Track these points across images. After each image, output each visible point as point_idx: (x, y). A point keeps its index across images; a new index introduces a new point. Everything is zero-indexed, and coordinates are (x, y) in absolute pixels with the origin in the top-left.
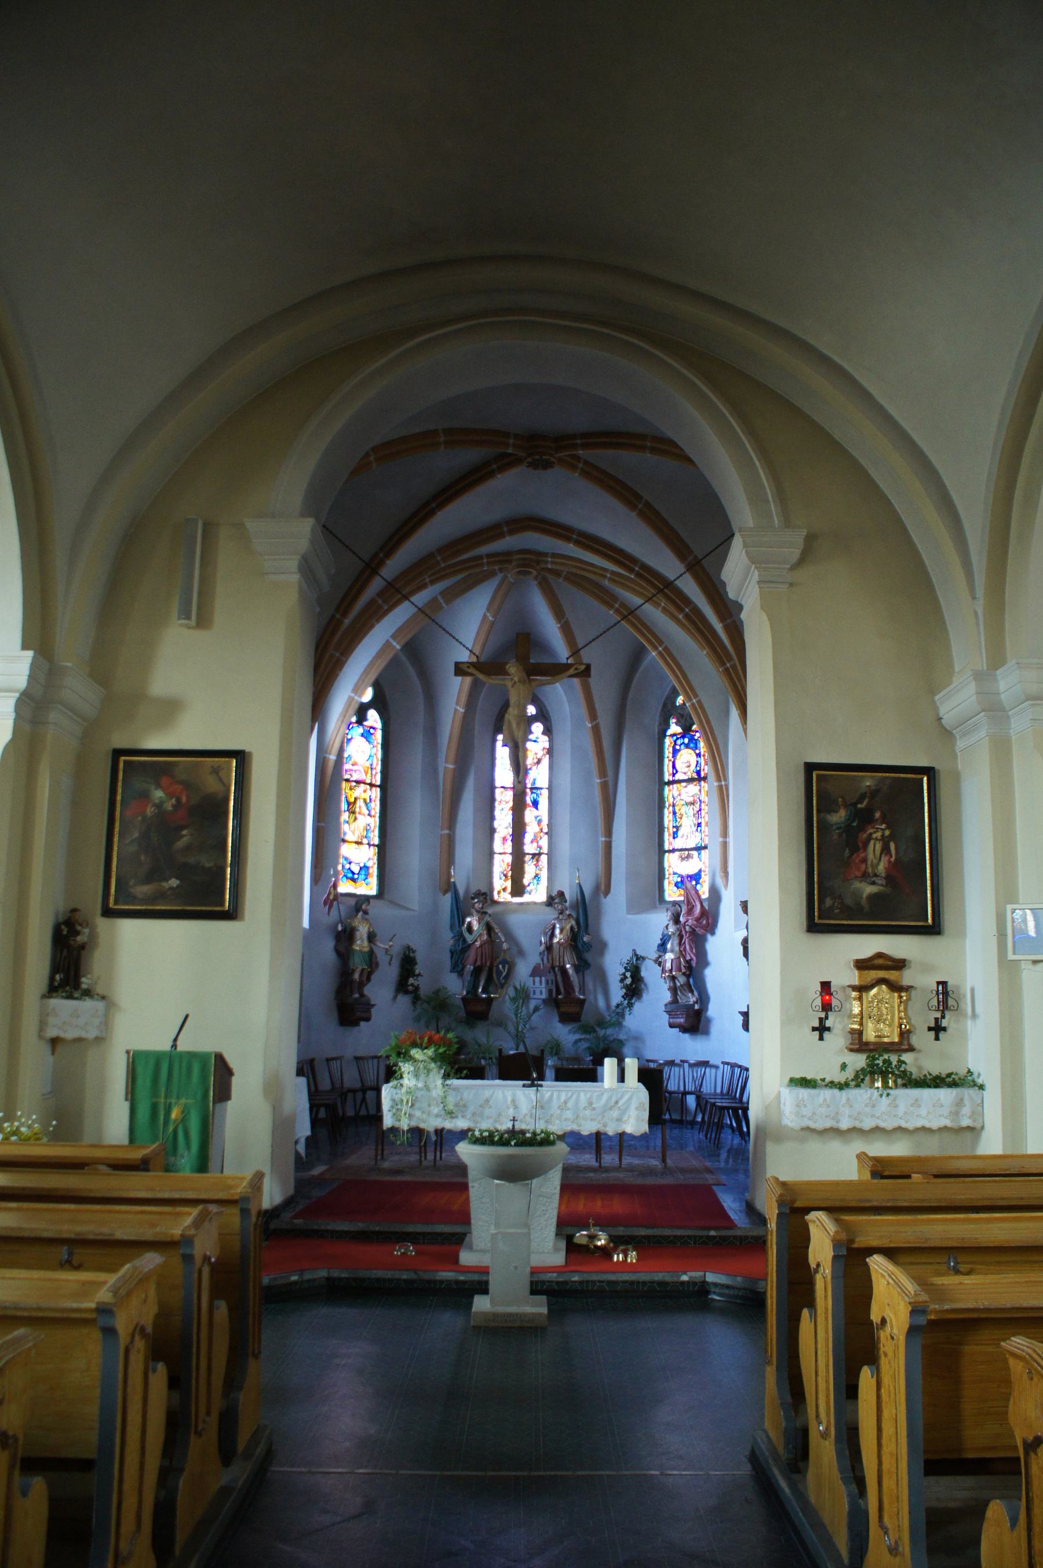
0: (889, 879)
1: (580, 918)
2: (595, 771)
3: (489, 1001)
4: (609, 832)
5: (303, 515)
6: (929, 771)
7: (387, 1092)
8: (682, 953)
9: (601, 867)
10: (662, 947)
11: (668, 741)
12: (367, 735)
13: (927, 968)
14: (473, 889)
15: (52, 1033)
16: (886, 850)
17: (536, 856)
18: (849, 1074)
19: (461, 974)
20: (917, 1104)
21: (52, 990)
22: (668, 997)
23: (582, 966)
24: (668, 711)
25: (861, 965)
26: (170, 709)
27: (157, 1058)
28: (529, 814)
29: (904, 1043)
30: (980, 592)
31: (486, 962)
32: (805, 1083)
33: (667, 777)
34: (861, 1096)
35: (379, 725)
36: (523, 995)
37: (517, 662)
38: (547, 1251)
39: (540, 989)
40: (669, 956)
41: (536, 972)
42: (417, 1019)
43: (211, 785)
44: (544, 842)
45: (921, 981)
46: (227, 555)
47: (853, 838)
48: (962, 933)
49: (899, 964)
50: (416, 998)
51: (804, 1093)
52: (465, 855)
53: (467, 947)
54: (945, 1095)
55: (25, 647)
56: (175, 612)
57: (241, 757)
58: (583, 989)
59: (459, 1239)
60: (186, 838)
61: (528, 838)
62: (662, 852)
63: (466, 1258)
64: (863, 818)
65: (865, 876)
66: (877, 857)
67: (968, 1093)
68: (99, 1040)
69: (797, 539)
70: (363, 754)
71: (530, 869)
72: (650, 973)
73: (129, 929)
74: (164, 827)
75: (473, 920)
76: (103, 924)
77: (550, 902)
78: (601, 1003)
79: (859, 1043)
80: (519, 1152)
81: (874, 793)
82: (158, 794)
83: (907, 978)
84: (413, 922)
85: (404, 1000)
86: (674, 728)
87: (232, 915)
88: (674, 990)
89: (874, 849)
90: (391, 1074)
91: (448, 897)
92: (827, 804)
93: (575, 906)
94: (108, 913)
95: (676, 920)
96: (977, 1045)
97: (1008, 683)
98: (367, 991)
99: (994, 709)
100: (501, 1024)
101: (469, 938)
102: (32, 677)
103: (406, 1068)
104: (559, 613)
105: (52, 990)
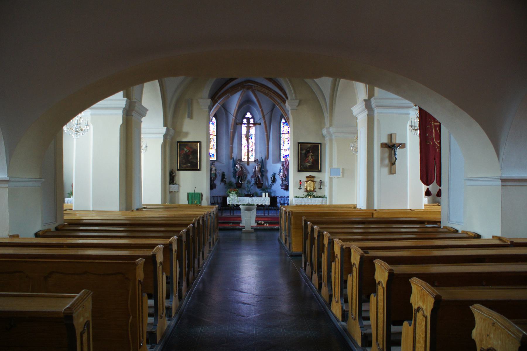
0: (312, 163)
1: (262, 164)
2: (265, 131)
3: (242, 184)
4: (268, 145)
5: (208, 98)
6: (320, 144)
7: (228, 199)
8: (284, 173)
9: (266, 154)
10: (280, 172)
11: (282, 124)
12: (213, 123)
13: (319, 178)
14: (238, 159)
15: (171, 190)
16: (312, 157)
17: (252, 150)
18: (304, 195)
19: (235, 178)
20: (315, 201)
21: (170, 183)
22: (281, 182)
23: (262, 175)
24: (282, 117)
25: (307, 177)
26: (187, 134)
27: (192, 193)
28: (250, 141)
29: (314, 190)
30: (328, 111)
31: (241, 175)
32: (297, 197)
33: (282, 132)
34: (306, 199)
35: (215, 121)
36: (249, 182)
37: (245, 105)
38: (254, 224)
39: (253, 181)
40: (281, 173)
41: (252, 177)
42: (226, 188)
43: (195, 147)
44: (254, 147)
45: (317, 180)
46: (195, 106)
47: (306, 155)
48: (325, 172)
49: (314, 177)
50: (225, 183)
51: (296, 199)
52: (235, 151)
53: (236, 172)
54: (320, 199)
55: (124, 97)
56: (187, 116)
57: (200, 142)
58: (262, 181)
59: (239, 223)
60: (191, 157)
61: (250, 146)
62: (280, 150)
63: (241, 225)
64: (308, 152)
65: (308, 162)
66: (310, 159)
67: (324, 199)
68: (178, 192)
69: (298, 101)
70: (213, 128)
71: (250, 153)
72: (277, 177)
73: (182, 173)
74: (187, 155)
75: (238, 166)
76: (177, 172)
77: (255, 161)
78: (267, 184)
79: (306, 191)
80: (249, 207)
81: (310, 148)
82: (186, 149)
83: (315, 180)
84: (225, 166)
85: (223, 184)
86: (283, 121)
87: (199, 170)
88: (282, 181)
89: (310, 157)
90: (228, 196)
91: (232, 160)
92: (302, 150)
93: (261, 162)
94: (178, 170)
95: (283, 165)
96: (326, 191)
97: (332, 130)
98: (215, 182)
99: (329, 133)
100: (244, 189)
101: (237, 170)
102: (126, 104)
103: (231, 195)
104: (256, 97)
105: (170, 183)
